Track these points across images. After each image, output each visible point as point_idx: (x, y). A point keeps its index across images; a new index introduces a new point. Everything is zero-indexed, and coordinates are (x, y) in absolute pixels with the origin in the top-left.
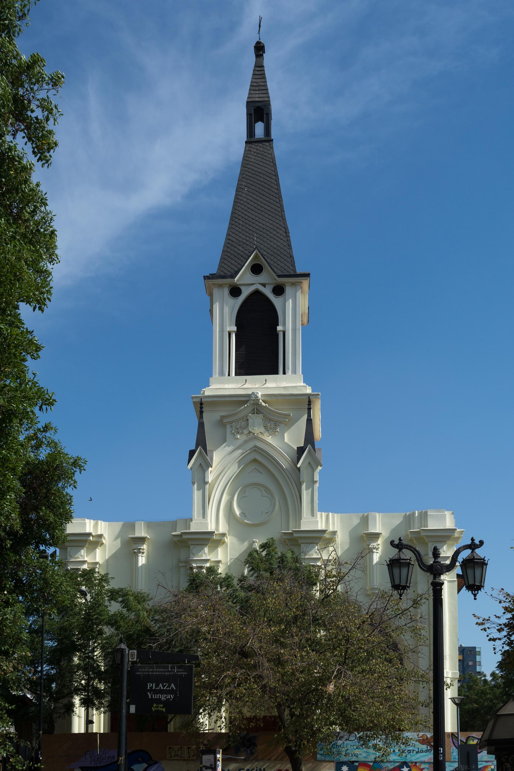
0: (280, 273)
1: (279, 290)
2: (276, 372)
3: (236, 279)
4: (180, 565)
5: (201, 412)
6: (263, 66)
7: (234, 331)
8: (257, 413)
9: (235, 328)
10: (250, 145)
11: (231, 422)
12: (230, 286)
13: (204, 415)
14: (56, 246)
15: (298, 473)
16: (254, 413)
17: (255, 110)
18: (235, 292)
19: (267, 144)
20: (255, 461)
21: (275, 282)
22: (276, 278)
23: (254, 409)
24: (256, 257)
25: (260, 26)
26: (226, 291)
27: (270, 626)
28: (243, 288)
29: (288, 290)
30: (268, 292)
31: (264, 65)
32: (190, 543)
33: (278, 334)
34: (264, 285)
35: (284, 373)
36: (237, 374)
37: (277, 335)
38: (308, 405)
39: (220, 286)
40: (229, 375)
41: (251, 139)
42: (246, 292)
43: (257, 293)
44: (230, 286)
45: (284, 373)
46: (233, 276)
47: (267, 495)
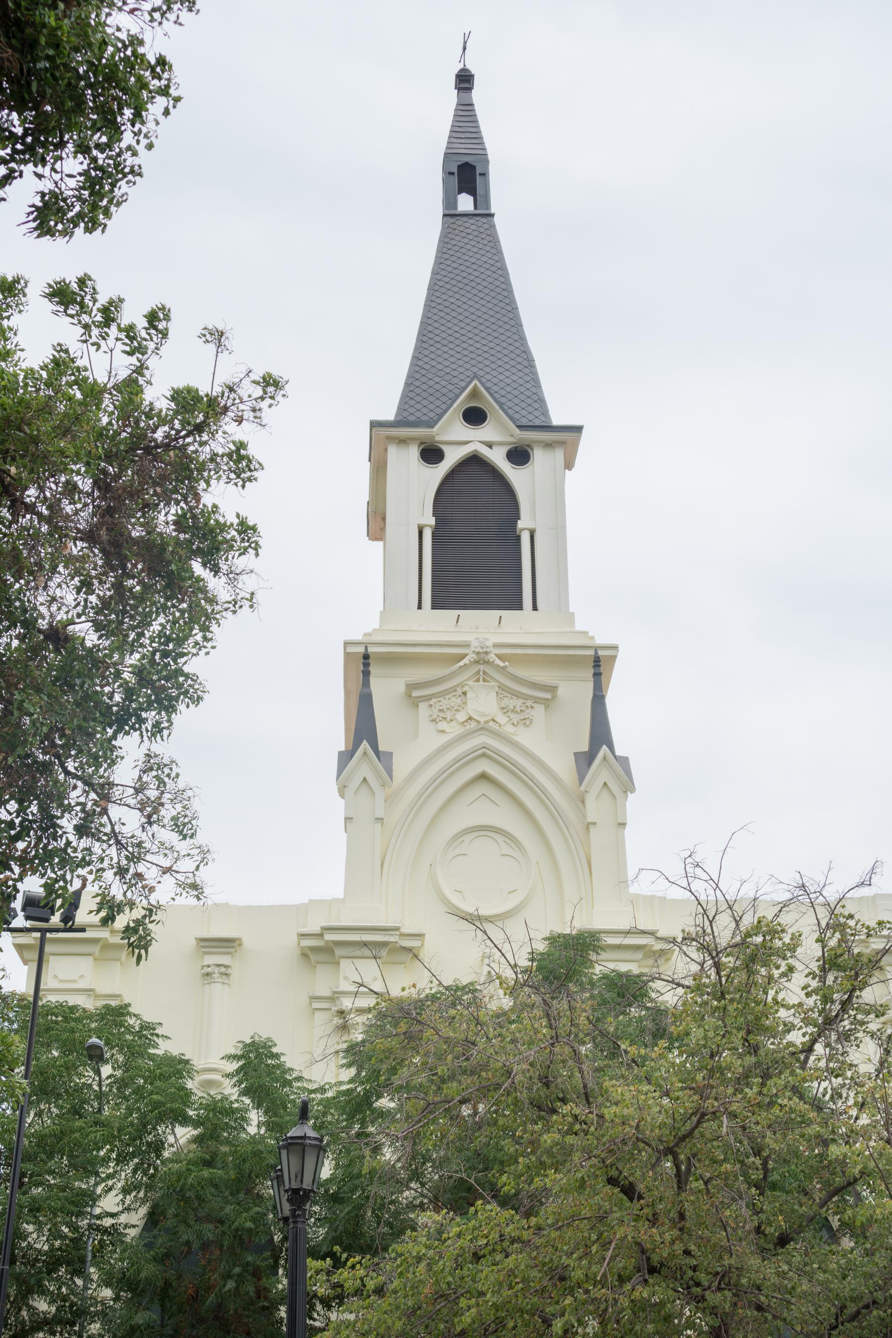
0: (524, 422)
1: (519, 455)
2: (519, 606)
3: (435, 429)
4: (316, 1005)
5: (366, 674)
6: (472, 105)
7: (430, 526)
8: (484, 680)
9: (432, 521)
10: (452, 220)
11: (428, 698)
12: (422, 443)
13: (373, 681)
14: (148, 1027)
15: (580, 805)
16: (478, 680)
17: (459, 167)
18: (431, 454)
19: (484, 220)
20: (483, 777)
21: (513, 440)
22: (517, 430)
23: (478, 673)
24: (475, 394)
25: (465, 48)
26: (414, 452)
27: (139, 845)
28: (446, 449)
29: (538, 455)
30: (498, 458)
31: (475, 102)
32: (339, 952)
33: (519, 537)
34: (490, 445)
35: (535, 608)
36: (434, 607)
37: (518, 538)
38: (594, 666)
39: (403, 442)
40: (420, 607)
41: (451, 215)
42: (452, 457)
43: (474, 461)
44: (422, 443)
45: (535, 608)
46: (431, 424)
47: (510, 852)
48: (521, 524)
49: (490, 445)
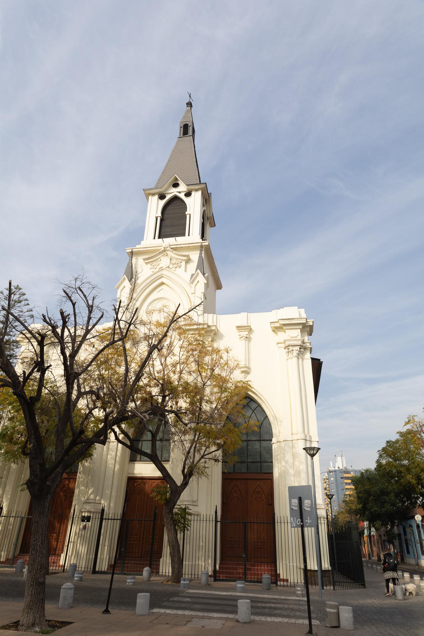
1: (188, 194)
18: (162, 197)
30: (182, 196)
34: (180, 192)
36: (159, 238)
42: (168, 197)
48: (186, 213)
49: (180, 192)
